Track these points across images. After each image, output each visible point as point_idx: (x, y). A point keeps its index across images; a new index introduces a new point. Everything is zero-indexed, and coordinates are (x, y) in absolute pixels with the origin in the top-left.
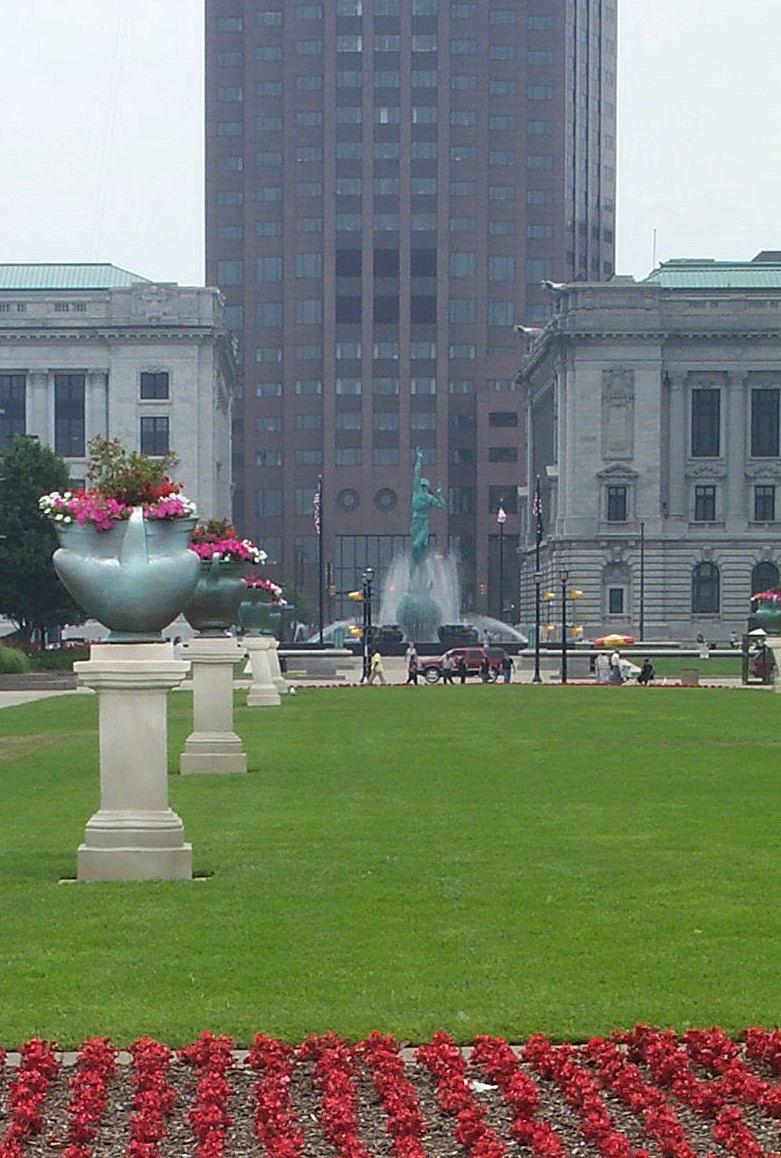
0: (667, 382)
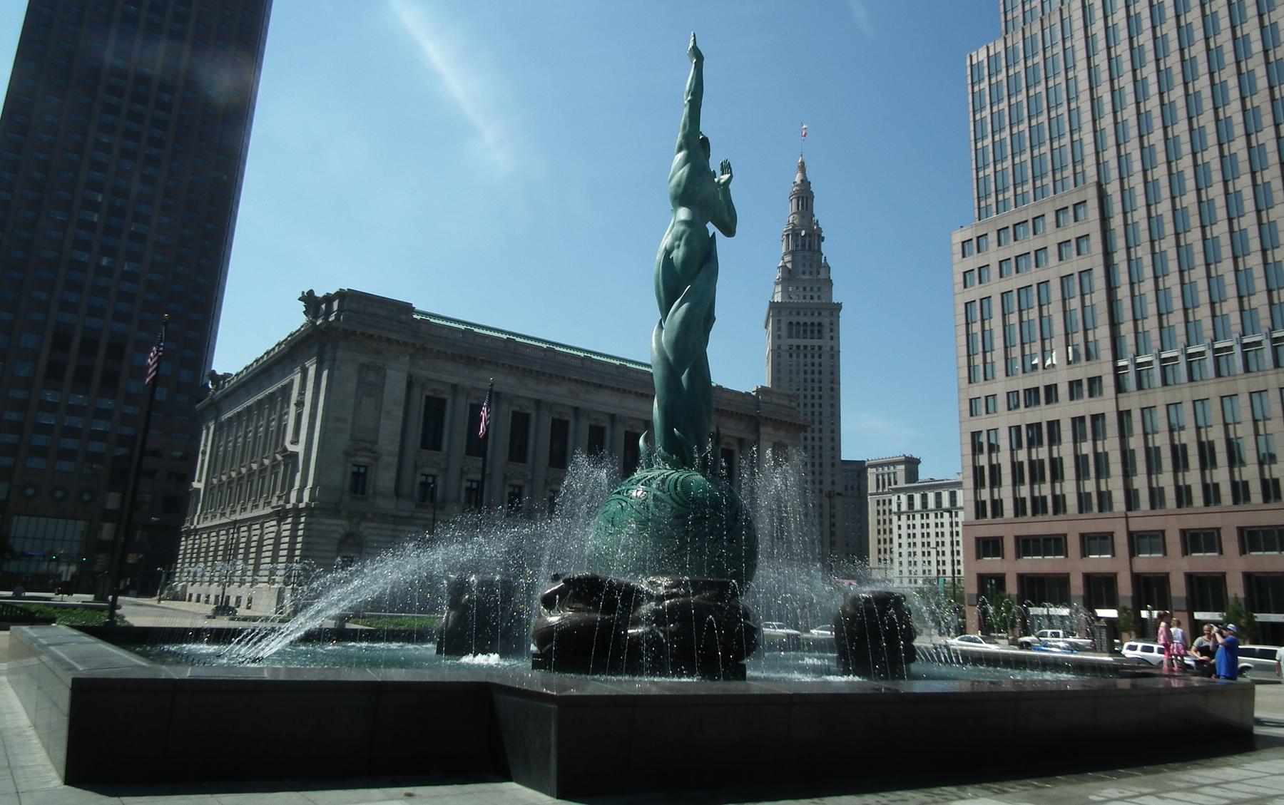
0: (410, 385)
